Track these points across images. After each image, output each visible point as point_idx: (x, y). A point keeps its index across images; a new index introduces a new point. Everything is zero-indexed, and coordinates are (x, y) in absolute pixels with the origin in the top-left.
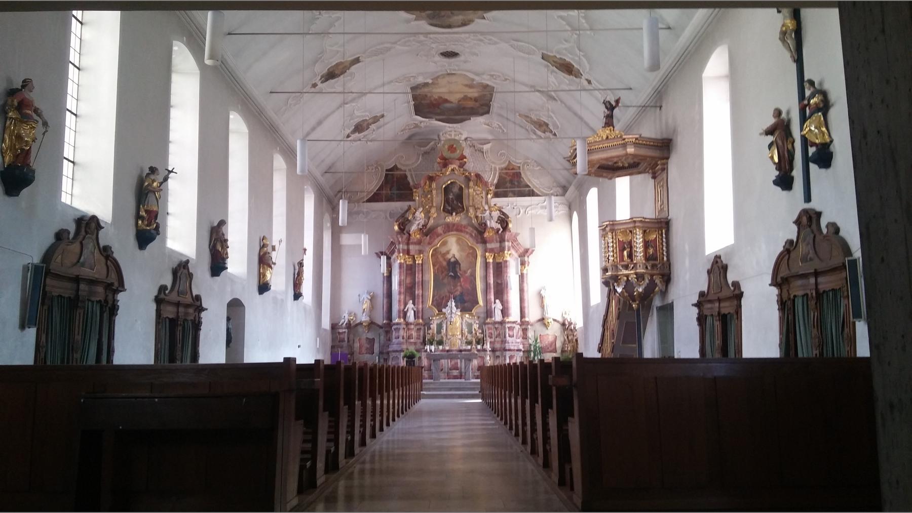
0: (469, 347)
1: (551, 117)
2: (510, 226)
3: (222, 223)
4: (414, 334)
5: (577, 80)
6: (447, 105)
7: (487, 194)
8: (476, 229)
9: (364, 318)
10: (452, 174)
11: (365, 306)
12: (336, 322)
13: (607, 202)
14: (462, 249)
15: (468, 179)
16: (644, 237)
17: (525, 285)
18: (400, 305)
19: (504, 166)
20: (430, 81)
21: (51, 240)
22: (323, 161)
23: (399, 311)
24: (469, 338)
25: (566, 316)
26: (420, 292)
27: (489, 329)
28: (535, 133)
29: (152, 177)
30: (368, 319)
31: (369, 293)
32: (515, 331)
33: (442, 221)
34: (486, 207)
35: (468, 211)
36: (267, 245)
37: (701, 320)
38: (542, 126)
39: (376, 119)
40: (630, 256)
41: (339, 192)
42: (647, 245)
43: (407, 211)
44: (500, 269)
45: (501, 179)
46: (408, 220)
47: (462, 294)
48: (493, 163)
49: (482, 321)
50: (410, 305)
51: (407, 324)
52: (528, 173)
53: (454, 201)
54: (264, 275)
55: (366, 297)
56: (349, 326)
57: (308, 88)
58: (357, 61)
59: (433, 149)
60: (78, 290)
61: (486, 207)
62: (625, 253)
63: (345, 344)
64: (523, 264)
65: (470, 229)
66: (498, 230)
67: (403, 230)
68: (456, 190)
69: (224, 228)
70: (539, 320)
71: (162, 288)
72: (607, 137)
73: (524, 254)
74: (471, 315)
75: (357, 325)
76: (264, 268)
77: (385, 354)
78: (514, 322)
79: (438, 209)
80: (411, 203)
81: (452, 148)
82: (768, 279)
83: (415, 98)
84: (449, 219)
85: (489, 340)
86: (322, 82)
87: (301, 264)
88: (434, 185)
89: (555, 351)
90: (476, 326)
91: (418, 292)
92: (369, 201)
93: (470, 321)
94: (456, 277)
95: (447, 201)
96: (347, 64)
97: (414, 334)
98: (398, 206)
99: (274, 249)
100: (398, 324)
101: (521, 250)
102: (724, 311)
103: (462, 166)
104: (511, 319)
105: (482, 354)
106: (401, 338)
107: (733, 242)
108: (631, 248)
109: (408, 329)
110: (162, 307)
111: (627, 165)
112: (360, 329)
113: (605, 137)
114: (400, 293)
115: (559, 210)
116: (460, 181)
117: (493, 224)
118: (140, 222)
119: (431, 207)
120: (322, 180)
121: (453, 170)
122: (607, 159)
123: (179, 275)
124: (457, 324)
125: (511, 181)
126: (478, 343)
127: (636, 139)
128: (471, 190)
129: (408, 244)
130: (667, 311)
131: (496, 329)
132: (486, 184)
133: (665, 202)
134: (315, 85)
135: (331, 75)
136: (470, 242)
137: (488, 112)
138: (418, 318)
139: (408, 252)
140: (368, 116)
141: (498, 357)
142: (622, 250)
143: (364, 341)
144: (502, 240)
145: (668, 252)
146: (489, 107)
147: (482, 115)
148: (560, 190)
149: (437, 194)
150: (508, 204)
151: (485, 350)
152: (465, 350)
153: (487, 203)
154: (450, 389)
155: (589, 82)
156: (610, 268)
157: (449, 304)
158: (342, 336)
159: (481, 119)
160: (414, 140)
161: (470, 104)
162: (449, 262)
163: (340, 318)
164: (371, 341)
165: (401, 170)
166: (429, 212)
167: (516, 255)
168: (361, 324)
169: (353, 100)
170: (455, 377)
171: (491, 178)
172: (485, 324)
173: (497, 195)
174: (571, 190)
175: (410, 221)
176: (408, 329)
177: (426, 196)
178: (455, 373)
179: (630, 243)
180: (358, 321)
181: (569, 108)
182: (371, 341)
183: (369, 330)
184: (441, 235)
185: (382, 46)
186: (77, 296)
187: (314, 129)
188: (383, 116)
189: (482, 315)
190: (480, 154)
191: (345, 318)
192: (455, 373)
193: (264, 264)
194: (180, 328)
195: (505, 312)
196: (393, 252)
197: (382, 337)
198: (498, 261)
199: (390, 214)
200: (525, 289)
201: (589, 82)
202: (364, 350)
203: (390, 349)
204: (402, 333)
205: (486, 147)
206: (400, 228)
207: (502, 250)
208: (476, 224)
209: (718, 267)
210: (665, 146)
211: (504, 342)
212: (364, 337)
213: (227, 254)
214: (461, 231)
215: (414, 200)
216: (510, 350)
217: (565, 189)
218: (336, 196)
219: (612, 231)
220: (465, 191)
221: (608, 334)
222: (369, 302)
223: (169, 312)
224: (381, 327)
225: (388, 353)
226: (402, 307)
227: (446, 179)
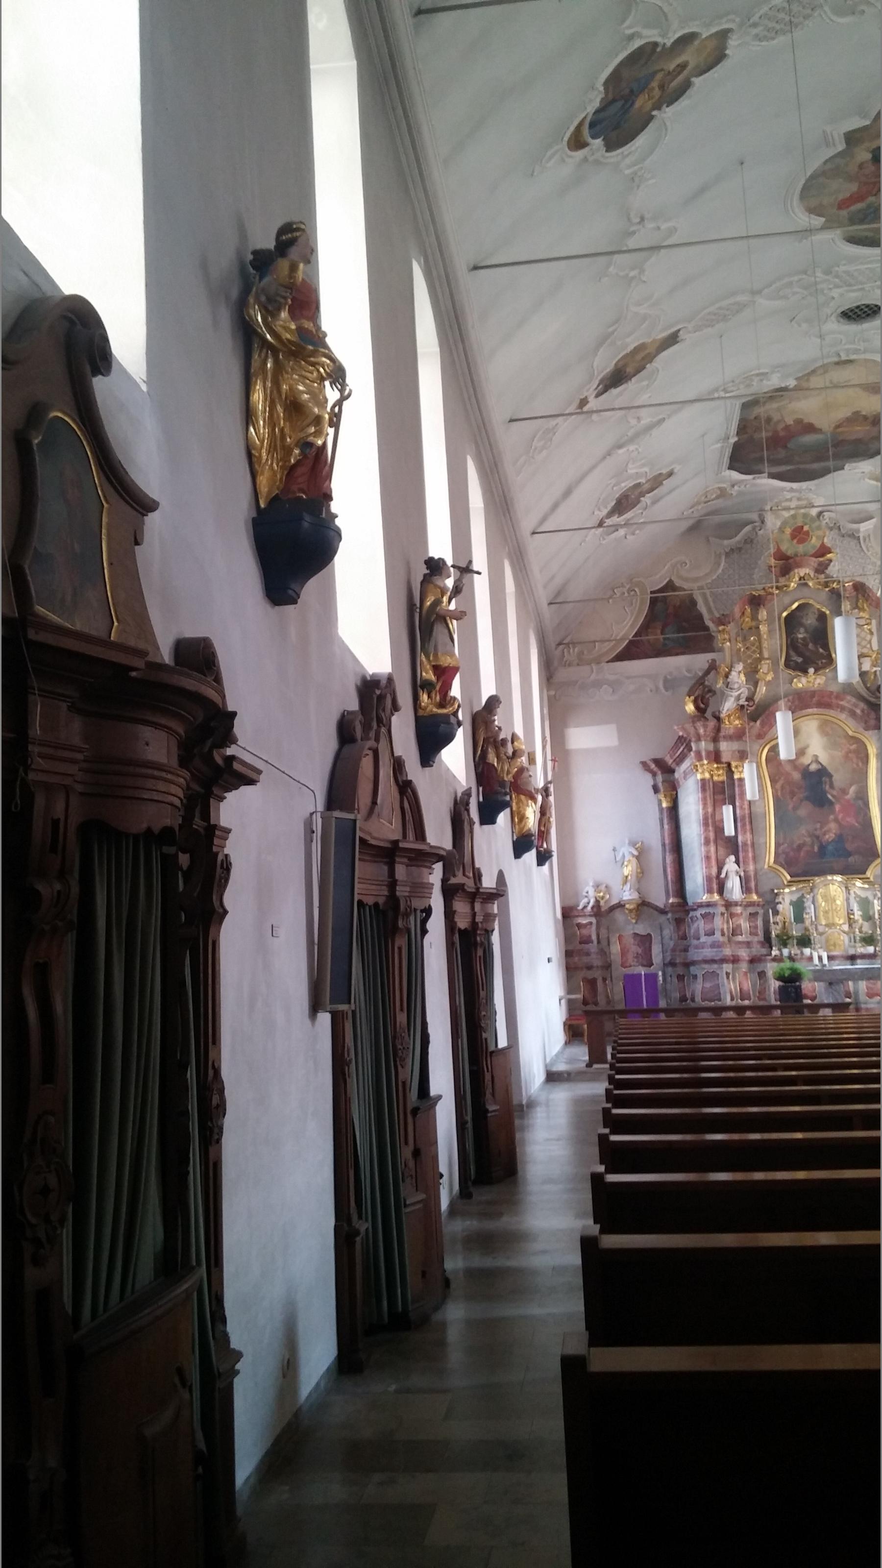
0: (871, 949)
6: (809, 439)
9: (628, 895)
10: (797, 591)
11: (626, 871)
12: (570, 903)
14: (832, 745)
15: (836, 596)
20: (792, 383)
21: (332, 744)
22: (553, 577)
23: (709, 879)
30: (635, 896)
31: (633, 844)
39: (657, 481)
41: (560, 644)
43: (707, 672)
47: (840, 838)
50: (730, 865)
51: (729, 905)
55: (627, 851)
56: (598, 911)
58: (673, 339)
59: (749, 541)
60: (392, 884)
63: (593, 947)
68: (810, 620)
74: (866, 880)
75: (613, 909)
79: (775, 663)
84: (800, 683)
88: (763, 614)
92: (622, 657)
93: (863, 894)
95: (792, 645)
96: (651, 350)
97: (745, 925)
100: (709, 905)
103: (821, 569)
106: (718, 934)
109: (732, 915)
112: (619, 916)
116: (820, 603)
118: (424, 697)
129: (715, 740)
134: (583, 402)
135: (617, 378)
136: (851, 727)
139: (716, 757)
143: (630, 941)
149: (770, 632)
152: (863, 957)
158: (585, 932)
162: (806, 773)
163: (577, 895)
164: (645, 941)
166: (756, 671)
168: (620, 906)
176: (732, 915)
177: (745, 639)
180: (614, 901)
182: (645, 941)
183: (638, 918)
185: (731, 300)
186: (393, 899)
188: (670, 474)
190: (853, 543)
191: (588, 897)
199: (666, 681)
202: (630, 959)
204: (719, 923)
205: (865, 528)
206: (697, 707)
214: (828, 706)
215: (721, 650)
222: (634, 861)
224: (663, 912)
225: (687, 965)
226: (714, 871)
227: (787, 600)
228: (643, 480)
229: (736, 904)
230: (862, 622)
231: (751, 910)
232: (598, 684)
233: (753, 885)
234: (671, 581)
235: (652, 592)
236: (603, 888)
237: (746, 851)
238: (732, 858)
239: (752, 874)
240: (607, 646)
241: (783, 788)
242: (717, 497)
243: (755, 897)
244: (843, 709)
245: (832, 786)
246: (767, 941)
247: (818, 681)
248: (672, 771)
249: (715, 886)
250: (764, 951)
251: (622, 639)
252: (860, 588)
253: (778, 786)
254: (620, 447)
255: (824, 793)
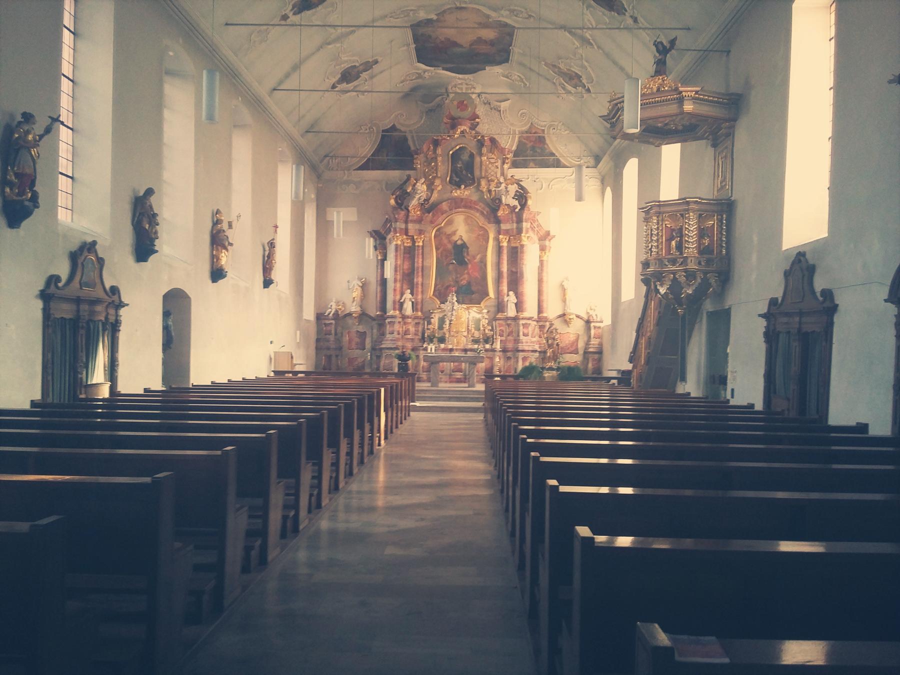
1: (585, 68)
2: (530, 202)
3: (150, 192)
4: (412, 329)
5: (620, 18)
7: (503, 163)
8: (488, 205)
9: (354, 308)
11: (354, 295)
13: (649, 176)
16: (699, 222)
17: (544, 274)
18: (395, 295)
19: (525, 128)
23: (394, 302)
24: (477, 334)
25: (591, 312)
26: (420, 279)
27: (500, 325)
28: (564, 88)
29: (26, 128)
32: (530, 329)
33: (447, 195)
34: (502, 180)
35: (479, 184)
36: (222, 221)
37: (770, 337)
38: (574, 79)
39: (368, 66)
40: (680, 247)
41: (326, 156)
42: (702, 233)
43: (405, 182)
44: (516, 254)
45: (520, 144)
46: (407, 193)
47: (469, 283)
48: (512, 124)
49: (492, 316)
50: (408, 295)
51: (404, 317)
52: (554, 139)
53: (464, 172)
54: (218, 259)
55: (356, 283)
57: (276, 21)
59: (439, 106)
61: (502, 180)
62: (673, 243)
63: (332, 338)
64: (543, 249)
65: (481, 206)
66: (515, 207)
67: (401, 204)
68: (465, 157)
69: (153, 200)
70: (560, 316)
71: (53, 280)
72: (658, 90)
73: (546, 236)
76: (217, 250)
77: (377, 351)
78: (530, 319)
79: (443, 180)
80: (411, 172)
81: (462, 105)
82: (884, 292)
83: (416, 39)
84: (457, 193)
85: (499, 338)
86: (294, 14)
87: (272, 245)
89: (576, 352)
90: (484, 322)
91: (418, 280)
92: (362, 168)
94: (462, 262)
95: (455, 171)
97: (412, 329)
98: (395, 175)
99: (230, 225)
100: (392, 317)
101: (542, 233)
102: (807, 328)
103: (473, 127)
104: (526, 314)
105: (490, 354)
106: (396, 333)
107: (825, 235)
108: (681, 236)
109: (405, 323)
110: (52, 304)
111: (680, 128)
113: (655, 90)
114: (395, 281)
115: (591, 184)
116: (472, 146)
117: (509, 200)
118: (8, 190)
119: (434, 178)
120: (302, 141)
121: (462, 132)
122: (656, 118)
123: (80, 261)
124: (466, 319)
125: (533, 148)
126: (486, 341)
127: (697, 92)
128: (484, 158)
129: (406, 222)
130: (721, 321)
131: (509, 325)
132: (502, 151)
133: (728, 176)
134: (285, 17)
136: (481, 221)
137: (506, 60)
138: (417, 310)
140: (357, 61)
141: (509, 358)
142: (669, 240)
143: (354, 335)
144: (519, 221)
145: (728, 242)
146: (508, 52)
147: (499, 63)
148: (592, 162)
149: (443, 162)
150: (529, 176)
151: (493, 350)
152: (471, 350)
153: (503, 174)
154: (450, 399)
155: (635, 20)
156: (652, 262)
157: (449, 298)
158: (329, 328)
159: (498, 69)
160: (424, 97)
161: (484, 49)
162: (455, 245)
164: (362, 335)
165: (401, 131)
166: (433, 183)
167: (535, 238)
168: (350, 314)
169: (338, 39)
170: (459, 381)
171: (509, 143)
172: (495, 319)
173: (515, 165)
174: (605, 160)
175: (409, 194)
176: (405, 323)
178: (459, 375)
179: (681, 230)
181: (607, 55)
182: (362, 335)
183: (360, 323)
184: (446, 212)
187: (287, 76)
189: (493, 309)
192: (459, 375)
193: (217, 245)
194: (83, 332)
195: (519, 306)
196: (388, 231)
197: (375, 331)
198: (513, 245)
199: (387, 184)
200: (545, 279)
201: (635, 20)
202: (354, 345)
203: (383, 346)
204: (397, 327)
205: (504, 105)
206: (396, 202)
207: (520, 231)
208: (489, 201)
209: (802, 266)
210: (734, 104)
211: (517, 341)
212: (354, 329)
213: (156, 233)
214: (470, 208)
215: (415, 169)
216: (523, 351)
217: (598, 159)
218: (322, 161)
219: (658, 214)
220: (477, 159)
221: (643, 341)
222: (360, 289)
223: (64, 311)
225: (381, 349)
226: (398, 297)
228: (357, 64)
229: (408, 317)
230: (493, 161)
231: (416, 321)
232: (348, 183)
233: (419, 307)
234: (394, 125)
235: (383, 131)
236: (341, 303)
237: (417, 287)
238: (409, 291)
239: (420, 300)
240: (355, 160)
241: (442, 253)
242: (417, 78)
243: (420, 314)
244: (478, 210)
245: (468, 254)
246: (423, 340)
247: (466, 193)
248: (385, 239)
249: (397, 306)
250: (420, 344)
251: (364, 157)
252: (493, 141)
253: (439, 251)
254: (329, 44)
255: (464, 257)
